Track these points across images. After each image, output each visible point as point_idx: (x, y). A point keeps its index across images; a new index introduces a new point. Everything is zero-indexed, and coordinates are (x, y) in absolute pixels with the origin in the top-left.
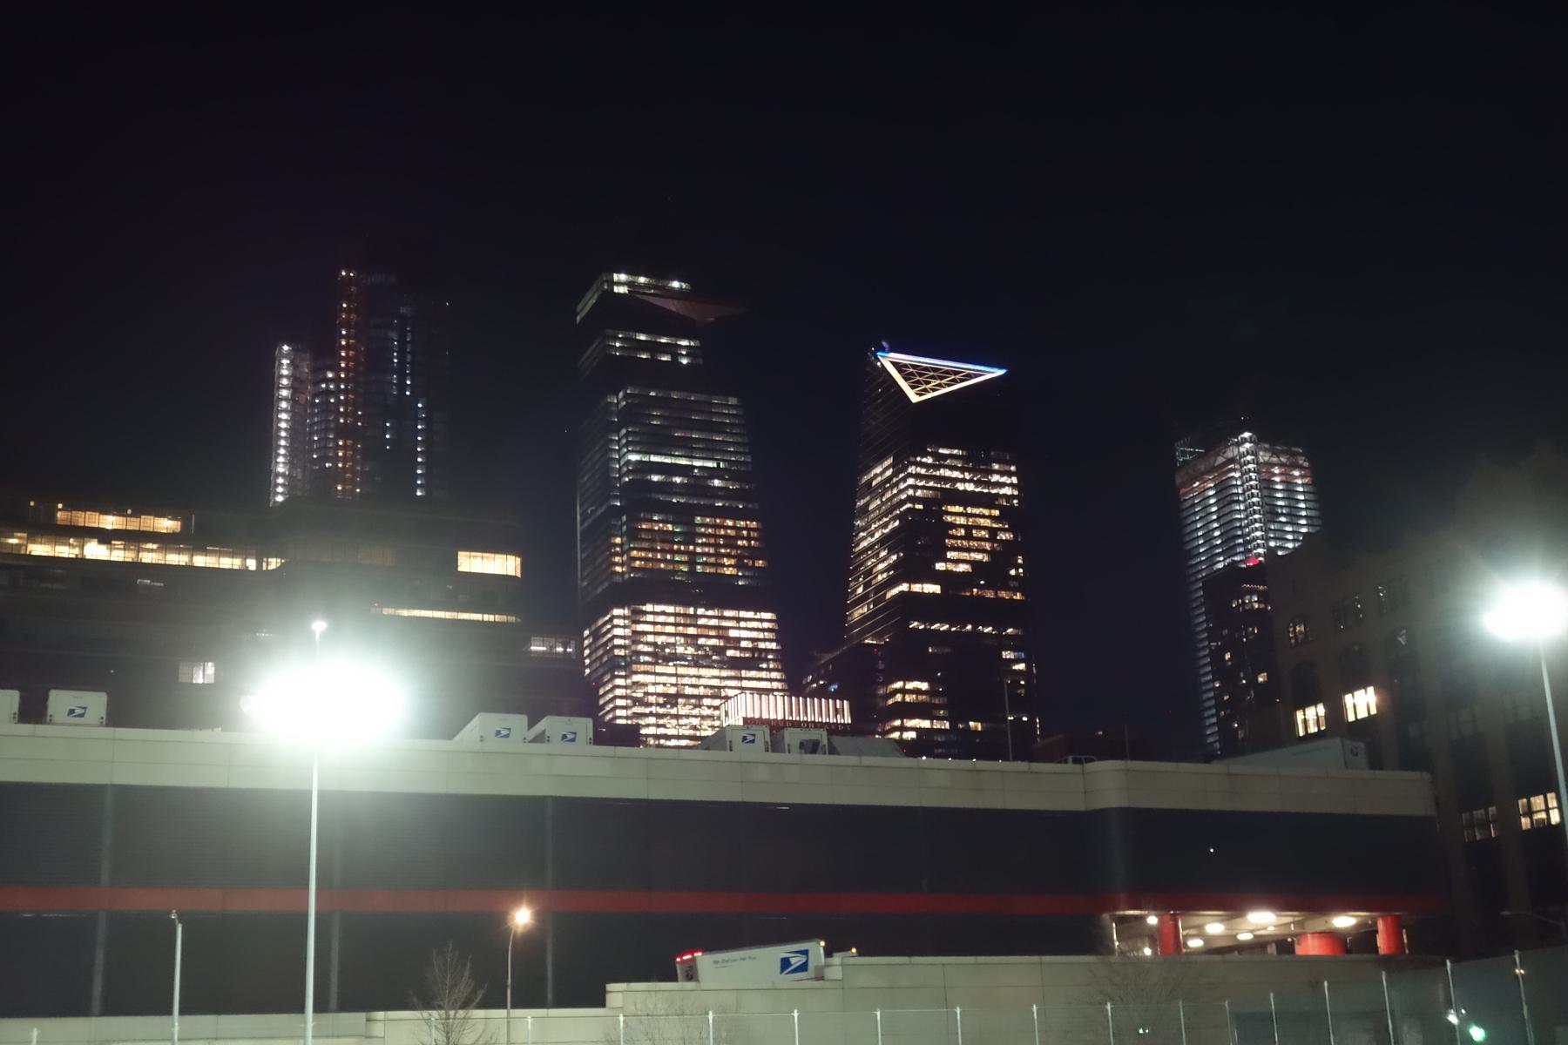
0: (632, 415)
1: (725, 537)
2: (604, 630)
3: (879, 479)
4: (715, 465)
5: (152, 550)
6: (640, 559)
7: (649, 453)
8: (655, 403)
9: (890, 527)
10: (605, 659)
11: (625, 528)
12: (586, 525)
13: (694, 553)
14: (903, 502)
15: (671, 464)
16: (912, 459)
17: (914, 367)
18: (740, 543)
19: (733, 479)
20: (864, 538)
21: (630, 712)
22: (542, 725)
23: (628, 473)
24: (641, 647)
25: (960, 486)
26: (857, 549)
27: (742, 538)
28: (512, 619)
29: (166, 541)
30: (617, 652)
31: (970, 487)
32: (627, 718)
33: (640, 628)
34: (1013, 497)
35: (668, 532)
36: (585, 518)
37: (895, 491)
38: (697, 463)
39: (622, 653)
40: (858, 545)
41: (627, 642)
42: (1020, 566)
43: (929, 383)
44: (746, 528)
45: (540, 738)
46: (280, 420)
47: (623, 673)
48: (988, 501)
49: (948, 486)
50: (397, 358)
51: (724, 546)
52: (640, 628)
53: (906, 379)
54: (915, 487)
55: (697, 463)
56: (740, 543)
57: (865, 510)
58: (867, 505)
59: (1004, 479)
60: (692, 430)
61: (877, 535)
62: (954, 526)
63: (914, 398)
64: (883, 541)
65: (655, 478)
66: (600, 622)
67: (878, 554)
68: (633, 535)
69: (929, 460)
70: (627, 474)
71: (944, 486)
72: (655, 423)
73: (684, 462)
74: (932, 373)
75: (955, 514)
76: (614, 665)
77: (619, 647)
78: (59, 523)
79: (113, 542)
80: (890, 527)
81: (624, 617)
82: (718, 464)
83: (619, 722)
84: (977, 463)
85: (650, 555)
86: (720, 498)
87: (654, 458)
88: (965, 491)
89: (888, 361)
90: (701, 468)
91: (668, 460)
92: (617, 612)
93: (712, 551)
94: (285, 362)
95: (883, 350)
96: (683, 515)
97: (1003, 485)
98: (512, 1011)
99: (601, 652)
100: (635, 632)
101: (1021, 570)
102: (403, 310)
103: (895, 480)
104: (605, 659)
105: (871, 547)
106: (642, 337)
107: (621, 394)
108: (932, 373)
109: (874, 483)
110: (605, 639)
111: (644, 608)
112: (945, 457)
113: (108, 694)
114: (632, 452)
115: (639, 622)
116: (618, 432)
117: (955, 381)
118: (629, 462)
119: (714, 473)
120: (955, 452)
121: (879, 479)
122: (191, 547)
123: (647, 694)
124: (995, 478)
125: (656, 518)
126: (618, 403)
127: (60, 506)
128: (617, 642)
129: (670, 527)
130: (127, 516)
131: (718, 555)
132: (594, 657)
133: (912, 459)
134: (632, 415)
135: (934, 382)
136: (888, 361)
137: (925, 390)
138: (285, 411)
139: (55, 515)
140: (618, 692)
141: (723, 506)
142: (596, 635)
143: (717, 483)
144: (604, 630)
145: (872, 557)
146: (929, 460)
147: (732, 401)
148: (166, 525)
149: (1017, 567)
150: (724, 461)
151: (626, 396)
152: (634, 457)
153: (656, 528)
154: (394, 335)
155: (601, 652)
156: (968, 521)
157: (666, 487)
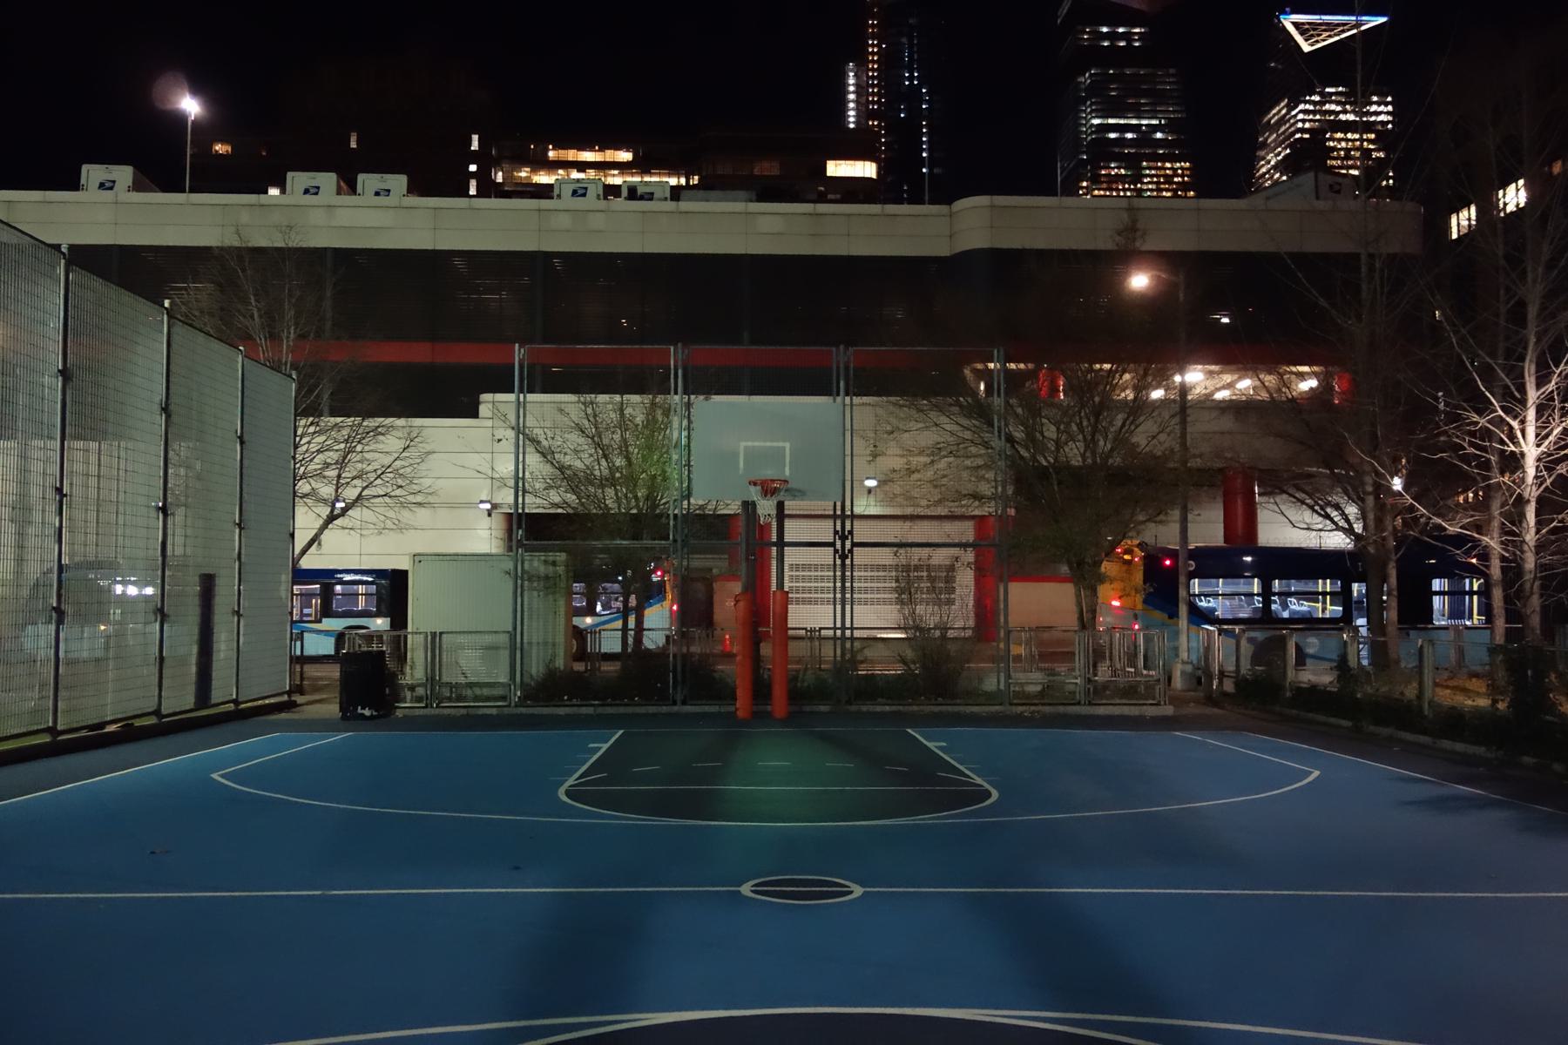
0: (1097, 89)
1: (1165, 176)
3: (1276, 118)
4: (1158, 122)
5: (614, 175)
7: (1108, 117)
8: (1113, 79)
9: (1282, 155)
12: (1064, 175)
13: (1141, 190)
14: (1293, 134)
15: (1125, 124)
16: (1302, 99)
17: (1309, 24)
18: (1176, 180)
19: (1171, 132)
20: (1263, 165)
23: (1092, 133)
25: (1343, 117)
26: (1258, 174)
27: (1178, 176)
29: (622, 167)
31: (1351, 117)
34: (1388, 122)
35: (1122, 175)
36: (1063, 169)
37: (1288, 125)
38: (1145, 122)
40: (1258, 172)
42: (1391, 178)
43: (1321, 35)
44: (1182, 168)
46: (849, 116)
48: (1369, 127)
49: (1332, 118)
50: (907, 57)
51: (1164, 183)
53: (1302, 34)
54: (1303, 121)
55: (1145, 122)
56: (1176, 180)
57: (1264, 145)
58: (1267, 139)
59: (1382, 108)
60: (1142, 97)
61: (1272, 163)
62: (1334, 149)
63: (1306, 48)
64: (1275, 167)
65: (1112, 136)
67: (1273, 176)
68: (1096, 180)
69: (1316, 98)
70: (1092, 133)
71: (1328, 118)
72: (1130, 101)
73: (1134, 122)
74: (1324, 27)
75: (1339, 141)
78: (550, 159)
79: (587, 171)
80: (1282, 155)
82: (1160, 121)
84: (1357, 99)
85: (1108, 193)
86: (1162, 147)
87: (1111, 121)
88: (1347, 121)
89: (1288, 22)
90: (1146, 125)
91: (1122, 122)
93: (1154, 187)
94: (851, 74)
95: (1286, 13)
96: (1133, 162)
97: (1377, 113)
98: (528, 395)
101: (1391, 181)
102: (911, 21)
103: (1288, 117)
105: (1268, 172)
106: (1105, 30)
107: (1087, 75)
108: (1324, 27)
109: (1272, 122)
112: (1331, 94)
113: (83, 163)
114: (1094, 117)
116: (1085, 104)
117: (1343, 31)
118: (1092, 125)
119: (1155, 128)
120: (1340, 89)
121: (1276, 118)
122: (639, 171)
124: (1374, 108)
125: (1113, 165)
126: (1086, 81)
127: (551, 147)
129: (1123, 171)
130: (595, 151)
131: (1159, 190)
133: (1302, 99)
134: (1097, 89)
135: (1325, 34)
136: (1288, 22)
137: (1317, 42)
138: (853, 109)
139: (546, 155)
141: (1164, 153)
143: (1159, 135)
145: (1268, 179)
146: (1316, 98)
147: (1172, 71)
148: (625, 156)
149: (1388, 178)
150: (1164, 118)
151: (1091, 75)
152: (1096, 121)
153: (1113, 173)
154: (904, 40)
156: (1347, 144)
157: (1121, 142)
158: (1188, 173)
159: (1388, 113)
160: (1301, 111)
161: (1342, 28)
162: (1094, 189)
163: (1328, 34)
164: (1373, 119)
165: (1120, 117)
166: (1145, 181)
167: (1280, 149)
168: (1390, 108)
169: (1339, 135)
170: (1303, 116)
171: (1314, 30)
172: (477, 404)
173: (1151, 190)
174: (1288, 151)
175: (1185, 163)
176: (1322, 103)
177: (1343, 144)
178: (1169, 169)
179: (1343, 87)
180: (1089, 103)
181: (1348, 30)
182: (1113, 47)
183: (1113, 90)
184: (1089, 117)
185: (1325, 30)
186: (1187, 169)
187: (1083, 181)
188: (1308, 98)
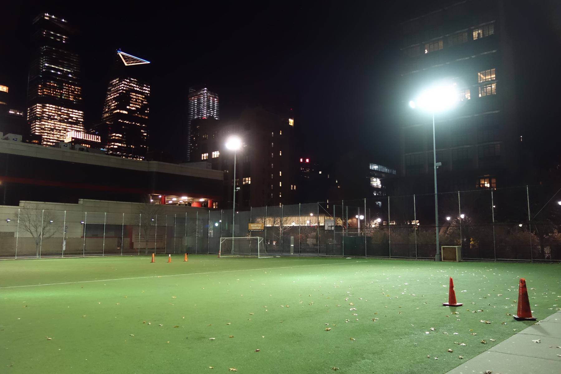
2: (34, 109)
4: (70, 71)
6: (46, 92)
10: (34, 117)
11: (42, 83)
19: (75, 76)
20: (109, 97)
21: (40, 131)
22: (6, 136)
24: (44, 115)
25: (135, 89)
27: (76, 91)
28: (4, 103)
30: (37, 115)
32: (39, 133)
33: (45, 110)
34: (148, 93)
35: (55, 86)
38: (65, 70)
39: (39, 116)
41: (40, 113)
42: (148, 110)
43: (130, 61)
44: (77, 89)
45: (7, 139)
47: (39, 121)
48: (142, 93)
52: (45, 110)
55: (65, 70)
57: (110, 90)
58: (111, 89)
59: (147, 89)
61: (113, 97)
62: (132, 98)
63: (126, 64)
66: (33, 107)
76: (35, 118)
77: (38, 114)
81: (40, 106)
82: (71, 71)
83: (36, 134)
84: (140, 84)
88: (136, 90)
92: (38, 105)
95: (119, 51)
99: (32, 115)
100: (43, 111)
104: (34, 117)
105: (111, 99)
109: (113, 84)
110: (34, 111)
111: (46, 105)
112: (132, 81)
115: (44, 108)
118: (45, 66)
120: (135, 80)
123: (45, 127)
124: (144, 88)
125: (52, 82)
128: (37, 112)
129: (56, 85)
132: (30, 116)
140: (37, 126)
142: (32, 110)
144: (34, 109)
147: (77, 55)
151: (46, 48)
152: (46, 65)
153: (52, 85)
155: (32, 115)
157: (56, 74)
158: (80, 91)
159: (148, 91)
160: (122, 86)
161: (136, 61)
162: (44, 89)
163: (133, 62)
164: (144, 91)
165: (56, 66)
166: (64, 90)
167: (115, 93)
168: (149, 89)
169: (134, 94)
170: (123, 86)
171: (128, 59)
172: (19, 203)
173: (66, 94)
174: (118, 95)
175: (79, 87)
176: (130, 83)
177: (135, 97)
178: (73, 88)
179: (136, 79)
180: (44, 57)
181: (139, 63)
182: (55, 40)
183: (54, 55)
184: (44, 62)
185: (131, 60)
186: (80, 90)
187: (39, 85)
188: (125, 80)
